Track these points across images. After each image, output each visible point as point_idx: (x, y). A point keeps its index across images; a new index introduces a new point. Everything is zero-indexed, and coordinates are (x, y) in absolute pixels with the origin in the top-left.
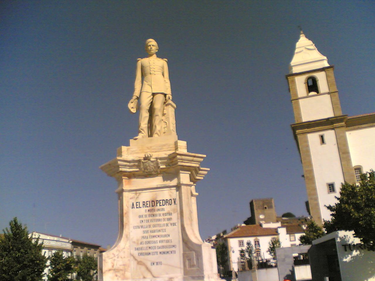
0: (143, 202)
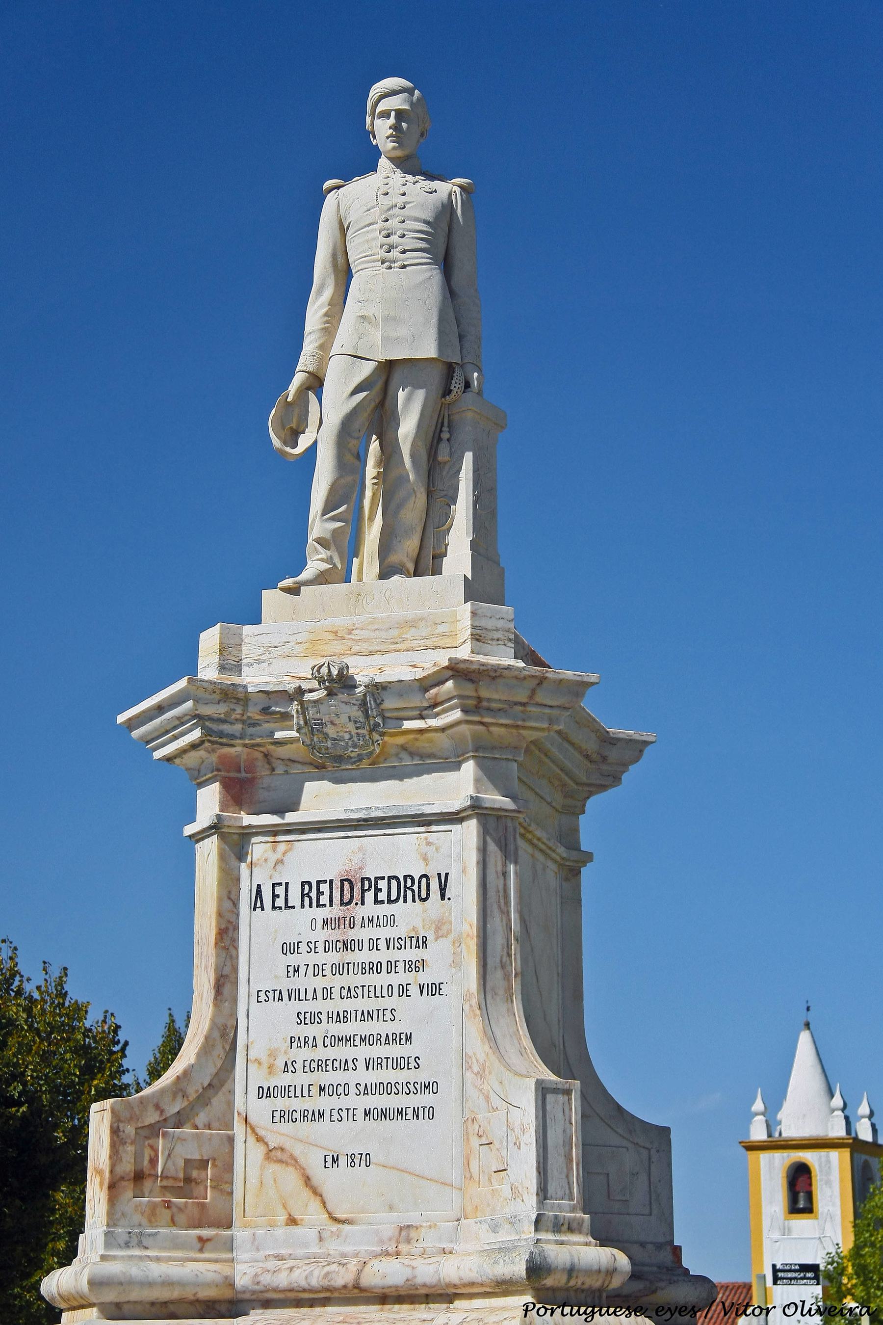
0: (303, 884)
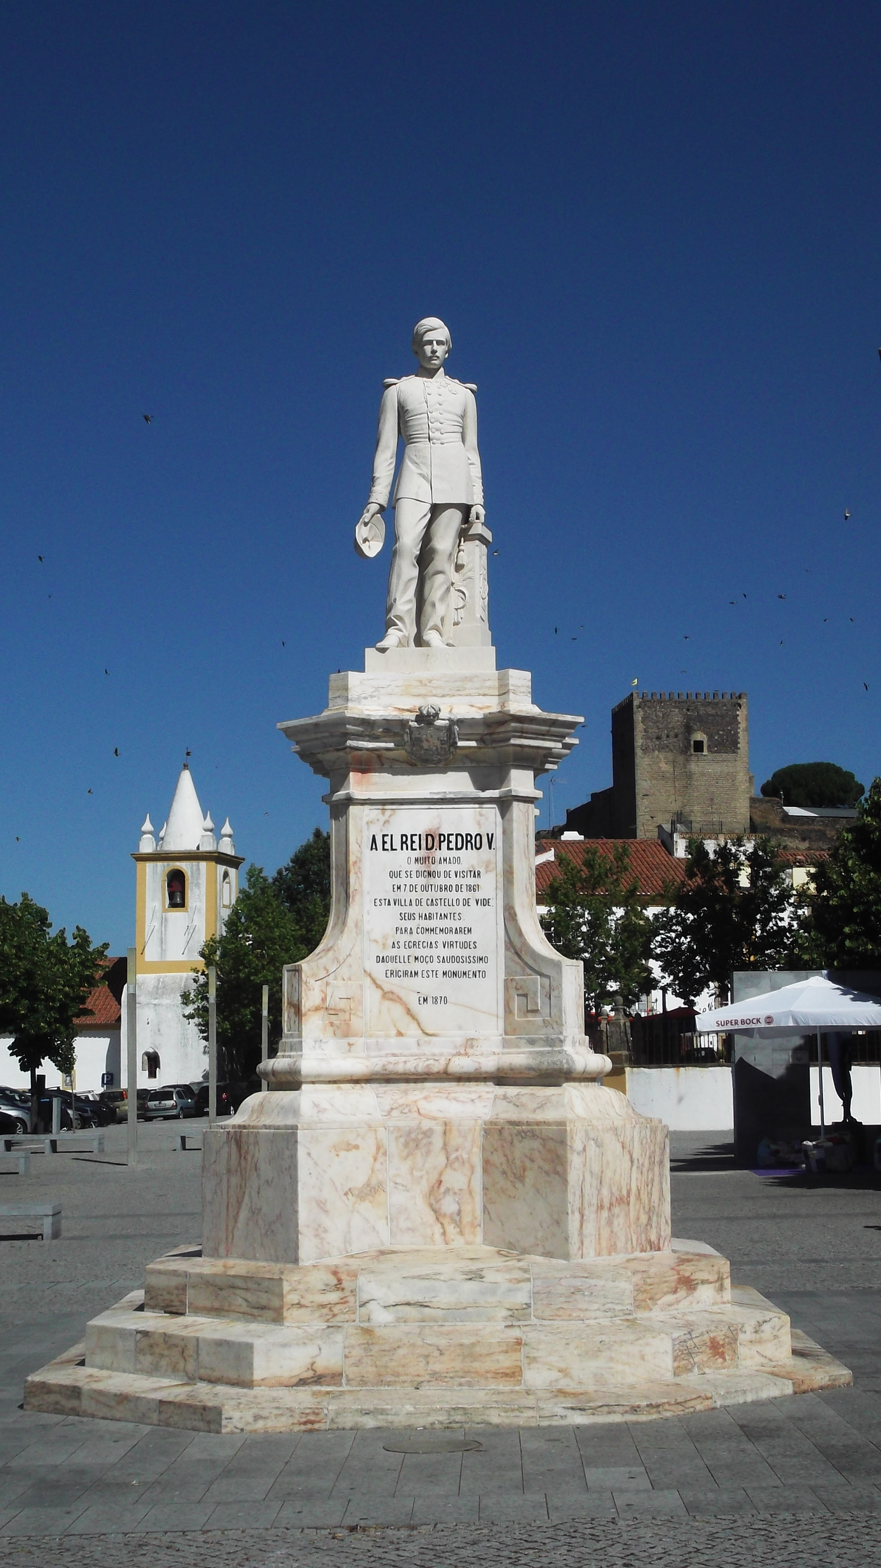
0: (402, 836)
